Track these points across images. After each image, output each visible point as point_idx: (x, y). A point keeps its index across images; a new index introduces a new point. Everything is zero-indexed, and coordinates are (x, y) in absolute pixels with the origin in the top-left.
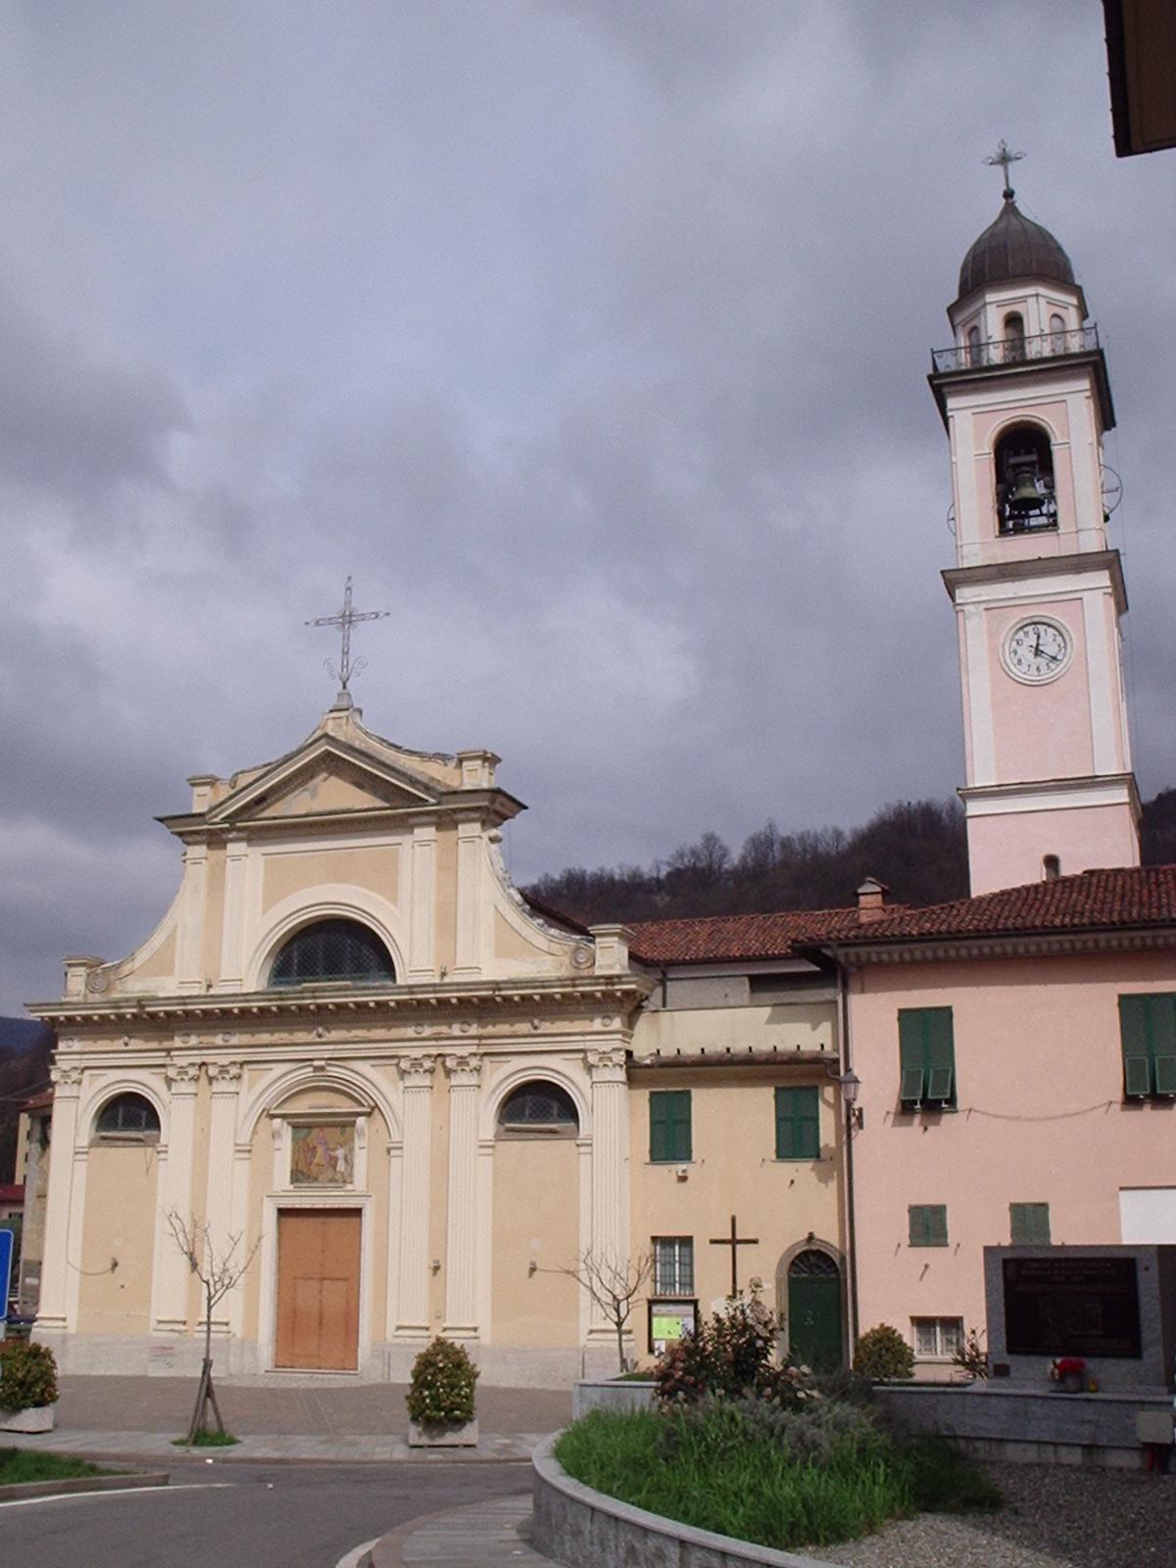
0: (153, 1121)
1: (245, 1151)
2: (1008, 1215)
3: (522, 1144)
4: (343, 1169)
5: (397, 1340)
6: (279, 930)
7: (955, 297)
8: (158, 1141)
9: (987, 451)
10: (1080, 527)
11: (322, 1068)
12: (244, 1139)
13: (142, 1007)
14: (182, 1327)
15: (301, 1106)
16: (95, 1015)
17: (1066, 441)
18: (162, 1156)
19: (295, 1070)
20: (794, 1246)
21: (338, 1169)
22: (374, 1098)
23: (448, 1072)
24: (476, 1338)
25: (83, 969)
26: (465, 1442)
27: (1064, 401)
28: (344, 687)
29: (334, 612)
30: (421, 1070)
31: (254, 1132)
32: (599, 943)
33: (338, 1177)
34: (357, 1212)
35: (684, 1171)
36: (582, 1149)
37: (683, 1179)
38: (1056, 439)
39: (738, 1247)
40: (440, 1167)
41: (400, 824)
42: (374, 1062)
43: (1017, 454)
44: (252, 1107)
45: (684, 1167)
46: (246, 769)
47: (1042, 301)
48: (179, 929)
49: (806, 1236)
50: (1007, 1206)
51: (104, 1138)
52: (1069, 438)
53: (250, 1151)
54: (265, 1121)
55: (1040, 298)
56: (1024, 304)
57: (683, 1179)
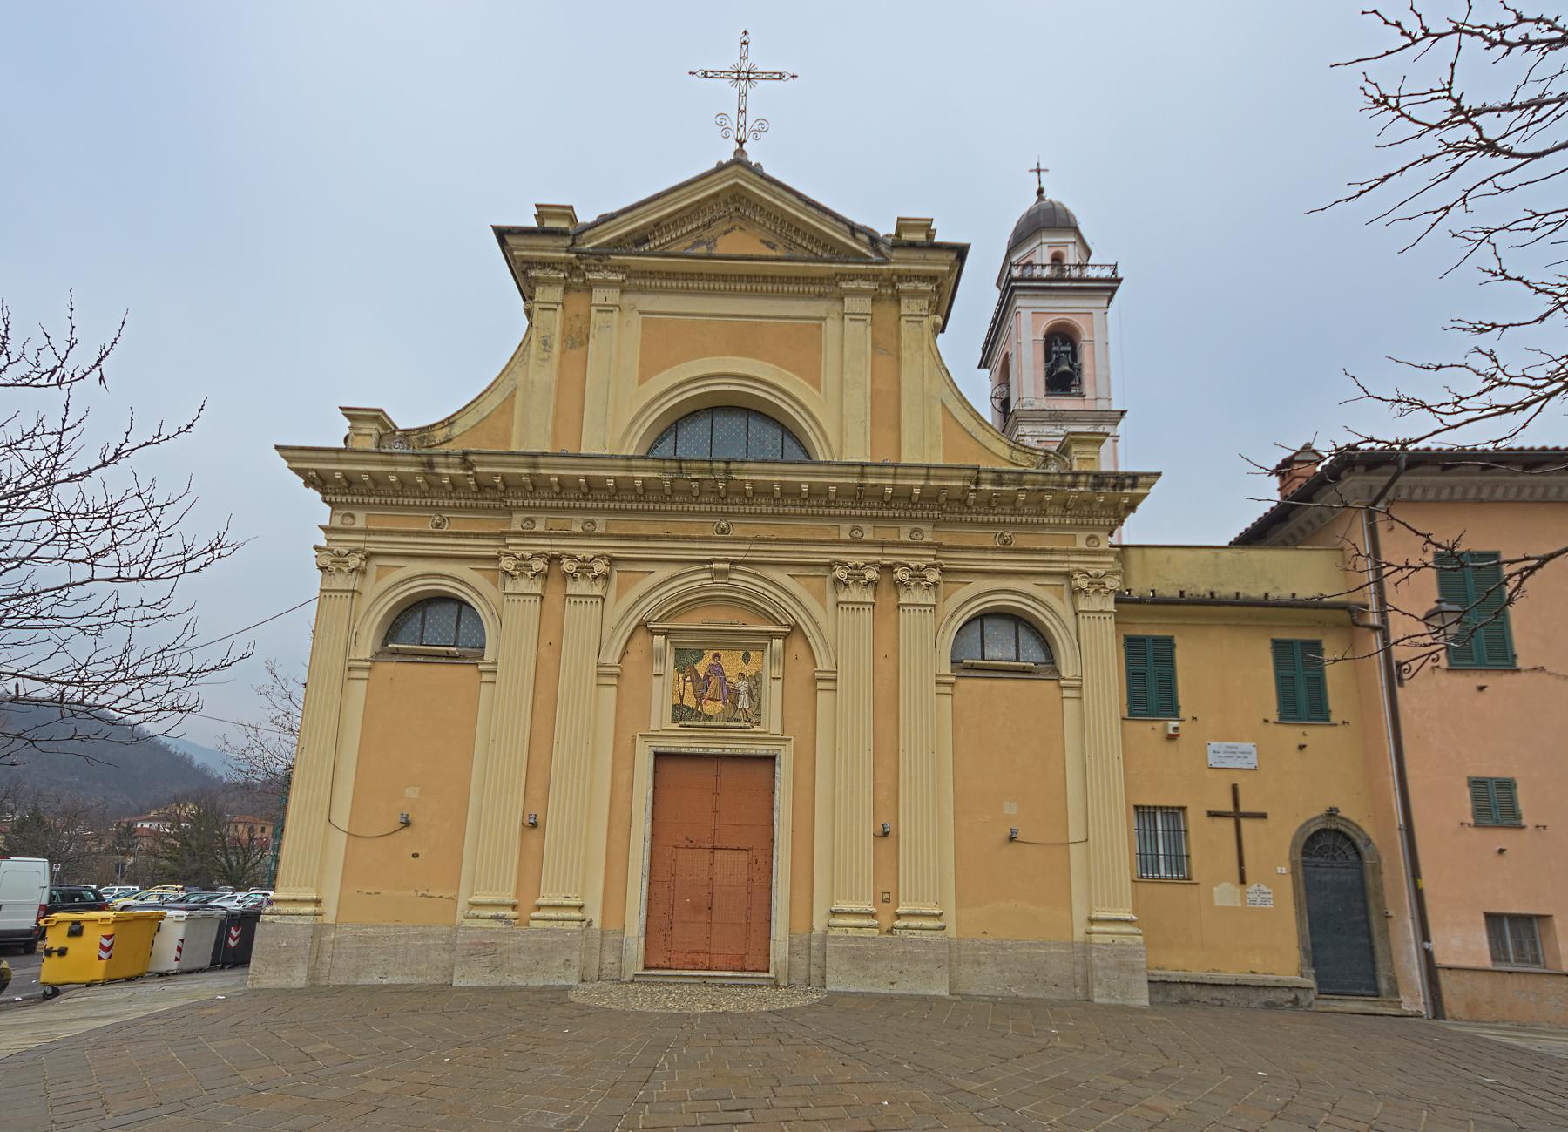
1: (612, 675)
3: (987, 683)
4: (746, 706)
6: (663, 405)
8: (482, 657)
10: (1098, 395)
11: (725, 573)
12: (611, 657)
13: (470, 466)
14: (510, 913)
16: (393, 473)
19: (672, 579)
20: (1308, 822)
23: (897, 585)
25: (376, 426)
27: (1091, 313)
31: (625, 652)
32: (1076, 452)
33: (740, 715)
34: (771, 760)
35: (1175, 729)
37: (1172, 738)
40: (887, 706)
41: (829, 288)
42: (794, 571)
44: (623, 619)
48: (518, 394)
53: (618, 676)
54: (641, 636)
57: (1172, 738)
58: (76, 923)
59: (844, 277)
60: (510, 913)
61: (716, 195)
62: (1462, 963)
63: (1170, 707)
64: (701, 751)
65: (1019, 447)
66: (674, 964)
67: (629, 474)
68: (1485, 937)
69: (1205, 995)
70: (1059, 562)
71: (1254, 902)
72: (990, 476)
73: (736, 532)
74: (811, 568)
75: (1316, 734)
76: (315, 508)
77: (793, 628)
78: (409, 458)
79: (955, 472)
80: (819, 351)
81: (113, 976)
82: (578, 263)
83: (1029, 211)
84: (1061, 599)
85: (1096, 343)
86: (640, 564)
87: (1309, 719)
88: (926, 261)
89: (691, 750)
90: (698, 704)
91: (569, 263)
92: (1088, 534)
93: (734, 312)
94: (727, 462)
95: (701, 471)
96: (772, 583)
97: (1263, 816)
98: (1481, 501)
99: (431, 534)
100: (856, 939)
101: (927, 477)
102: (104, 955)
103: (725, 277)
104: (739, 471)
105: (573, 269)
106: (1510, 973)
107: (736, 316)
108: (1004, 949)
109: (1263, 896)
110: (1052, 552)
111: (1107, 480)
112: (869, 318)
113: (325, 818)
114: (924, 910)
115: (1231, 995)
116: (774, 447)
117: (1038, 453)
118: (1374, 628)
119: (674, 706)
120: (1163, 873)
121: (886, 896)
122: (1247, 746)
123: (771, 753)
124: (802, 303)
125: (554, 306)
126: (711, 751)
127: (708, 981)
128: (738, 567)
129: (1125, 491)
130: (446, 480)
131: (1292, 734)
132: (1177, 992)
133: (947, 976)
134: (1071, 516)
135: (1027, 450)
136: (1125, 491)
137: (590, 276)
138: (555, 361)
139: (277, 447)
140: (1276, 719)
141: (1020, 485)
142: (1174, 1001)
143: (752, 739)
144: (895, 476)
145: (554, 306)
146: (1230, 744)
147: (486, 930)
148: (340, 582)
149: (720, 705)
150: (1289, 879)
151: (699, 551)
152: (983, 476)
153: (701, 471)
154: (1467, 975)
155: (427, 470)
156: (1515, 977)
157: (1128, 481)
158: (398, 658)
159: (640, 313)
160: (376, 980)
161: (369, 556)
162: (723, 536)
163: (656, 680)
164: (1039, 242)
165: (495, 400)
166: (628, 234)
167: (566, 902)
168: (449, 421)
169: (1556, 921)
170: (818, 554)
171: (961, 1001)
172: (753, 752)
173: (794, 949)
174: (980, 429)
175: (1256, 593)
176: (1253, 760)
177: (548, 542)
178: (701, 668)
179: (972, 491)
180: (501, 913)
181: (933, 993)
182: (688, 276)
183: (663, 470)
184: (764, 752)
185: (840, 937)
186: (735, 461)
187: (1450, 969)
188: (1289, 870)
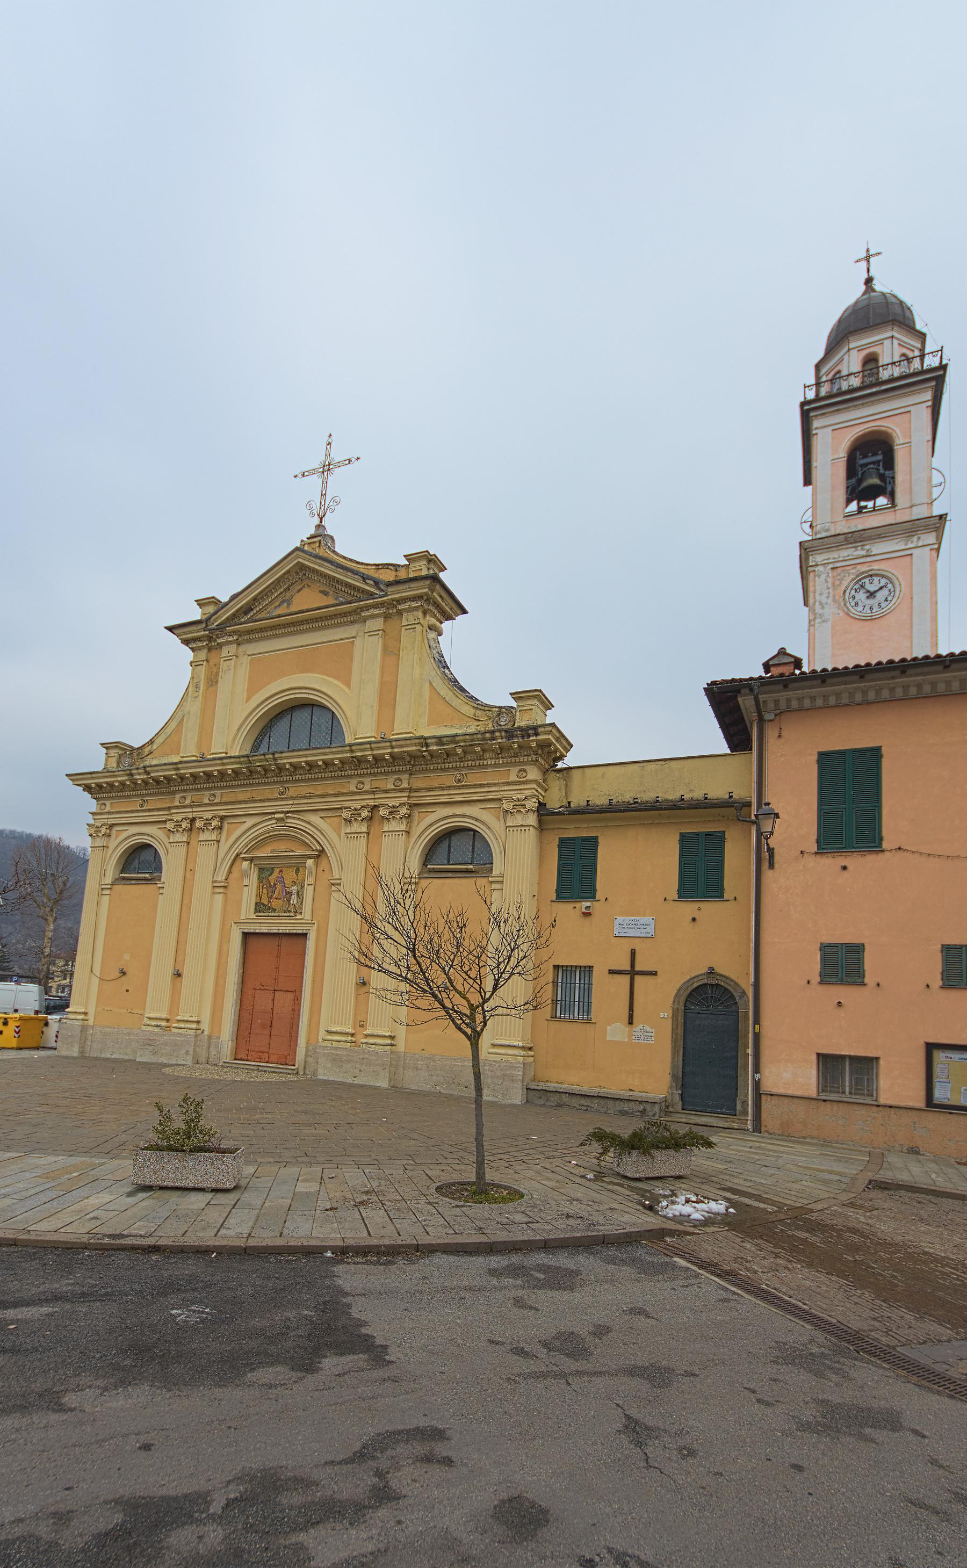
0: (156, 865)
2: (938, 958)
5: (326, 1043)
7: (821, 354)
8: (160, 880)
9: (842, 456)
10: (915, 501)
11: (282, 819)
12: (221, 876)
13: (148, 773)
15: (265, 852)
16: (116, 781)
17: (907, 440)
18: (161, 891)
21: (291, 902)
22: (322, 844)
24: (392, 1045)
25: (117, 751)
26: (214, 1185)
28: (321, 522)
29: (316, 464)
30: (359, 819)
31: (230, 872)
33: (291, 908)
35: (587, 908)
36: (494, 886)
37: (587, 914)
38: (899, 440)
39: (637, 978)
41: (354, 617)
43: (865, 456)
45: (588, 904)
46: (402, 861)
47: (896, 342)
48: (185, 718)
49: (705, 970)
50: (939, 946)
51: (124, 879)
52: (910, 438)
53: (225, 887)
55: (894, 340)
56: (881, 346)
57: (587, 914)
58: (6, 1019)
59: (362, 609)
60: (164, 1024)
61: (288, 572)
62: (790, 1092)
63: (588, 891)
64: (266, 931)
65: (480, 707)
66: (250, 1058)
67: (224, 767)
68: (814, 1072)
69: (574, 1102)
70: (495, 791)
71: (639, 1038)
72: (433, 740)
73: (291, 793)
74: (328, 812)
75: (709, 909)
76: (90, 803)
77: (320, 851)
78: (122, 773)
79: (408, 742)
80: (352, 660)
81: (22, 1046)
82: (211, 635)
83: (856, 303)
84: (498, 819)
85: (912, 444)
86: (239, 818)
87: (705, 897)
88: (411, 589)
89: (262, 931)
90: (270, 902)
91: (207, 636)
92: (519, 768)
93: (301, 644)
94: (273, 754)
95: (261, 761)
96: (299, 819)
97: (654, 973)
98: (869, 703)
99: (138, 811)
100: (336, 1048)
101: (392, 747)
102: (17, 1036)
103: (293, 624)
104: (281, 758)
105: (210, 639)
106: (824, 1101)
107: (302, 646)
108: (434, 1061)
109: (646, 1034)
110: (488, 785)
111: (515, 733)
112: (380, 633)
113: (89, 970)
114: (380, 1033)
115: (595, 1104)
116: (327, 728)
117: (494, 709)
118: (753, 822)
119: (256, 904)
120: (576, 1015)
121: (362, 1023)
122: (647, 919)
123: (305, 932)
124: (342, 629)
125: (202, 663)
126: (272, 931)
127: (261, 1068)
128: (290, 815)
129: (531, 738)
130: (139, 782)
131: (689, 908)
132: (554, 1099)
133: (388, 1075)
134: (503, 758)
135: (486, 709)
136: (531, 738)
137: (219, 641)
138: (200, 696)
139: (67, 775)
140: (676, 897)
141: (456, 743)
142: (552, 1104)
143: (294, 923)
144: (372, 749)
145: (202, 663)
146: (632, 918)
147: (151, 1032)
148: (99, 842)
149: (281, 902)
150: (670, 1021)
151: (269, 807)
152: (429, 741)
153: (261, 761)
154: (786, 1100)
155: (131, 778)
156: (828, 1105)
157: (531, 732)
158: (124, 882)
159: (249, 655)
160: (109, 1056)
161: (111, 826)
162: (282, 797)
163: (246, 889)
164: (846, 349)
165: (173, 724)
166: (237, 611)
167: (190, 1019)
168: (151, 742)
169: (882, 1062)
170: (335, 802)
171: (396, 1090)
172: (295, 931)
173: (309, 1053)
174: (454, 697)
175: (673, 796)
176: (650, 930)
177: (190, 810)
178: (272, 879)
179: (425, 751)
180: (159, 1023)
181: (378, 1085)
182: (272, 628)
183: (241, 763)
184: (300, 932)
185: (326, 1047)
186: (277, 752)
187: (891, 1107)
188: (671, 1015)
